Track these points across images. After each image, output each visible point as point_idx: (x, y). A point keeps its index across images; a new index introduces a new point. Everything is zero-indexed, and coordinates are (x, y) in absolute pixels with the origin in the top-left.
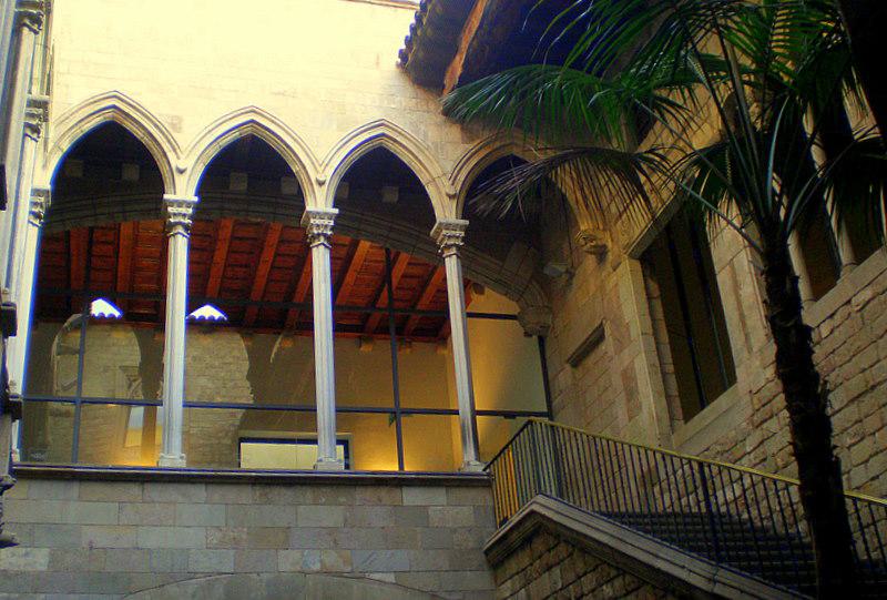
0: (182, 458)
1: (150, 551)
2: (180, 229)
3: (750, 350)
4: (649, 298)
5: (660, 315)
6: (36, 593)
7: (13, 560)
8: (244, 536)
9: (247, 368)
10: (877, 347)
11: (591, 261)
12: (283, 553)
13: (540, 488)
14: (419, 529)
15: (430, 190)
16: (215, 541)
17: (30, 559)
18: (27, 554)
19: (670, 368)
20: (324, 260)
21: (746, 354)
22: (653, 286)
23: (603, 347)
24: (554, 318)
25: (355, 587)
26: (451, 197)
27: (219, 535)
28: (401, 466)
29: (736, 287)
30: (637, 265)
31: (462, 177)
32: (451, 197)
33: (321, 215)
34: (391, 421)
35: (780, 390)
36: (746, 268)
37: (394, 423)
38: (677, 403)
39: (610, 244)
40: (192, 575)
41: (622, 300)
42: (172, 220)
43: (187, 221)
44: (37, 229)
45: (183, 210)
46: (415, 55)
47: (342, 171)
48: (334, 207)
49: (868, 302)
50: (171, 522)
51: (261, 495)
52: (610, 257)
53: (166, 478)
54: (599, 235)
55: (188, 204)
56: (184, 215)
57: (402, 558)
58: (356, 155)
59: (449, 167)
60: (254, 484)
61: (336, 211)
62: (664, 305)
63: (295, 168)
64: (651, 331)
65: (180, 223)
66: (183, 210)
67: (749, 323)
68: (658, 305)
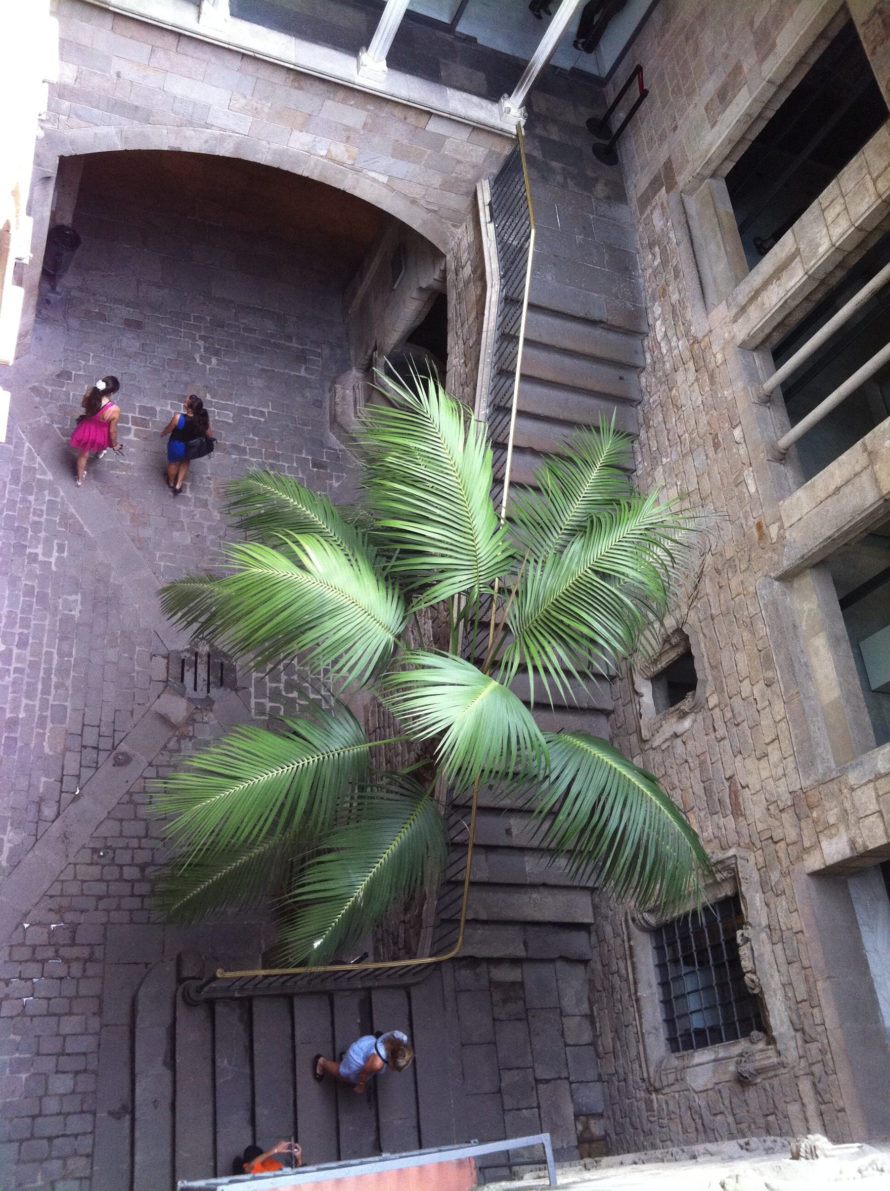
8: (266, 110)
12: (296, 133)
14: (429, 151)
16: (237, 106)
19: (770, 114)
25: (350, 176)
40: (208, 126)
57: (402, 168)
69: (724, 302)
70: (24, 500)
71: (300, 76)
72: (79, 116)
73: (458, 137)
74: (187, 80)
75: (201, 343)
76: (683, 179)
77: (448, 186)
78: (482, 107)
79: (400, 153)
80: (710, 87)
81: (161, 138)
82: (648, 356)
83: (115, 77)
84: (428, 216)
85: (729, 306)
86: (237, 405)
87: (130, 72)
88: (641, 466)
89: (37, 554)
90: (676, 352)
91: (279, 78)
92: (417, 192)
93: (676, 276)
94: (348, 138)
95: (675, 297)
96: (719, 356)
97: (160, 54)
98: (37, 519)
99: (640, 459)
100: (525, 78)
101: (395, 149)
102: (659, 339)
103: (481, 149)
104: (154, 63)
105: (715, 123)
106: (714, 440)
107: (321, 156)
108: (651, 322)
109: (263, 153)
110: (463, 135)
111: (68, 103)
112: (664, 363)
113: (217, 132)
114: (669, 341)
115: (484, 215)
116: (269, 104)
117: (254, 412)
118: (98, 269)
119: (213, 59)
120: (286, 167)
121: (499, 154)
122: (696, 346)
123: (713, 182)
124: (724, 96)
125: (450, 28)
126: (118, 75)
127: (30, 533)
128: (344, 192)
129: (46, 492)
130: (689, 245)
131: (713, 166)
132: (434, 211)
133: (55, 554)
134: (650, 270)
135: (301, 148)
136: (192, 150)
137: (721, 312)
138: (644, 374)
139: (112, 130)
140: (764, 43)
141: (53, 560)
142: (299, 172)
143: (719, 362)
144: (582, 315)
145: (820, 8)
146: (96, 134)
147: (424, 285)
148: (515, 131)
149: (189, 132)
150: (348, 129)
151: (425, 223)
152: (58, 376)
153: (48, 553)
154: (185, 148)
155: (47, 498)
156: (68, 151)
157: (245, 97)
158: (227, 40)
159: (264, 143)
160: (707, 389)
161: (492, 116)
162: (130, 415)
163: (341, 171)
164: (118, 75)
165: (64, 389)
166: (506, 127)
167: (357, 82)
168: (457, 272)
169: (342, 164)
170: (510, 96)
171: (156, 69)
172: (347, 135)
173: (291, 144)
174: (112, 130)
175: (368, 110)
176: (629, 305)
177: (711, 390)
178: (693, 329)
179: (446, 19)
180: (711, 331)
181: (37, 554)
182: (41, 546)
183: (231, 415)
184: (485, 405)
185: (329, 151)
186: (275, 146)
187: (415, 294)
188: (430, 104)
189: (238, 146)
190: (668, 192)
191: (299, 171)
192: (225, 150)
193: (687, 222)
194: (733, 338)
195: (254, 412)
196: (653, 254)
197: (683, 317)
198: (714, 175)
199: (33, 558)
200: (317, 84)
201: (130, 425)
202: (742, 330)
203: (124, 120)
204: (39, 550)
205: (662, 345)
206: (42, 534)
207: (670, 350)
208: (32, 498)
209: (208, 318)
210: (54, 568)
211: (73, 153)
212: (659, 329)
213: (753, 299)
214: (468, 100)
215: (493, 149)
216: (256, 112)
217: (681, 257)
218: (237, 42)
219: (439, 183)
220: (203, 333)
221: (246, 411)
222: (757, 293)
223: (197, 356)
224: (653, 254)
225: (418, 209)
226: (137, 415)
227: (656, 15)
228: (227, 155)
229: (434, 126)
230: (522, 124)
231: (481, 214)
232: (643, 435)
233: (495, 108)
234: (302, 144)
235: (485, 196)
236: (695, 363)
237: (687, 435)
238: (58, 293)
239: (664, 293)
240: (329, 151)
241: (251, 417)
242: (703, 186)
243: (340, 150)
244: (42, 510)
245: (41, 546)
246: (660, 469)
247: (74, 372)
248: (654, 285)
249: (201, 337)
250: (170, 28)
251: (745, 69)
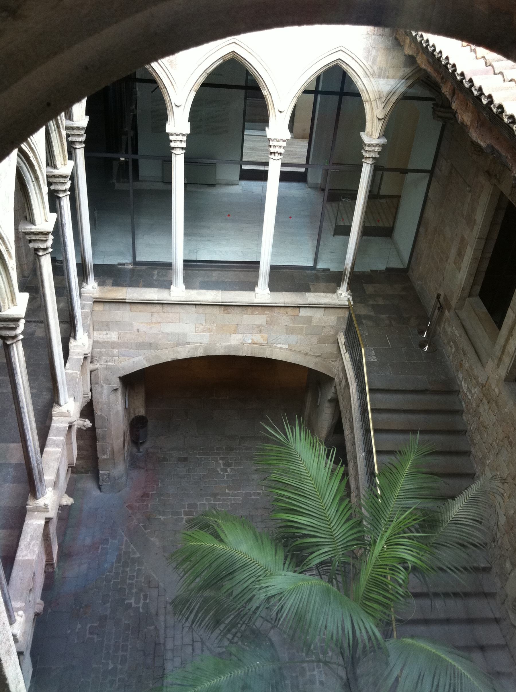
6: (114, 349)
7: (101, 336)
8: (214, 328)
12: (233, 336)
14: (305, 326)
16: (200, 330)
17: (109, 336)
18: (107, 334)
19: (489, 255)
20: (51, 290)
25: (267, 350)
35: (485, 237)
40: (188, 344)
44: (369, 166)
45: (180, 138)
57: (294, 338)
63: (265, 92)
66: (180, 138)
69: (490, 359)
70: (124, 571)
71: (226, 306)
72: (124, 355)
73: (318, 315)
74: (171, 324)
75: (221, 462)
76: (454, 302)
77: (322, 341)
78: (326, 297)
79: (290, 331)
80: (453, 252)
81: (167, 355)
82: (463, 403)
83: (136, 332)
84: (317, 359)
85: (493, 360)
86: (244, 492)
87: (143, 328)
88: (477, 470)
89: (131, 603)
90: (475, 395)
91: (216, 310)
92: (306, 348)
93: (465, 354)
94: (260, 331)
95: (467, 365)
96: (497, 390)
97: (155, 315)
98: (130, 581)
99: (476, 466)
100: (344, 276)
101: (287, 330)
102: (466, 392)
103: (333, 318)
104: (154, 320)
105: (460, 269)
106: (508, 440)
107: (250, 343)
108: (459, 383)
109: (219, 350)
110: (320, 313)
111: (117, 350)
112: (472, 404)
113: (193, 345)
114: (470, 391)
115: (343, 350)
116: (215, 325)
117: (254, 494)
118: (162, 435)
119: (182, 311)
120: (233, 354)
121: (344, 318)
122: (484, 389)
123: (471, 299)
124: (460, 254)
125: (314, 268)
126: (138, 330)
127: (127, 590)
128: (267, 358)
129: (136, 565)
130: (465, 335)
131: (467, 291)
132: (319, 356)
133: (142, 601)
134: (451, 356)
135: (237, 342)
136: (183, 358)
137: (490, 365)
138: (464, 414)
139: (141, 358)
140: (470, 221)
141: (140, 605)
142: (240, 355)
143: (498, 393)
144: (412, 389)
145: (490, 196)
146: (134, 362)
147: (329, 398)
148: (347, 303)
149: (179, 349)
150: (259, 326)
151: (316, 363)
152: (142, 496)
153: (137, 602)
154: (179, 358)
155: (137, 568)
156: (122, 373)
157: (203, 325)
158: (184, 300)
159: (218, 344)
160: (496, 411)
161: (333, 300)
162: (183, 510)
163: (262, 348)
164: (138, 330)
165: (145, 503)
166: (341, 303)
167: (255, 302)
168: (340, 384)
169: (261, 344)
170: (340, 287)
171: (155, 323)
172: (260, 329)
173: (232, 342)
174: (141, 358)
175: (266, 314)
176: (443, 377)
177: (499, 411)
178: (480, 380)
179: (311, 264)
180: (488, 378)
181: (131, 603)
182: (133, 598)
183: (241, 499)
184: (361, 451)
185: (253, 340)
186: (224, 345)
187: (327, 405)
188: (296, 303)
189: (205, 349)
190: (449, 312)
191: (240, 354)
192: (200, 353)
193: (462, 324)
194: (500, 377)
195: (254, 494)
196: (451, 347)
197: (473, 375)
198: (470, 295)
199: (129, 606)
200: (236, 308)
201: (183, 516)
202: (503, 372)
203: (145, 352)
204: (133, 601)
205: (468, 394)
206: (134, 591)
207: (472, 396)
208: (128, 569)
209: (224, 447)
210: (141, 610)
211: (125, 374)
212: (464, 386)
213: (503, 352)
214: (318, 296)
215: (339, 316)
216: (210, 330)
217: (464, 344)
218: (190, 299)
219: (317, 341)
220: (222, 456)
221: (250, 495)
222: (504, 347)
223: (219, 470)
224: (451, 347)
225: (309, 357)
226: (186, 510)
227: (422, 230)
228: (201, 355)
229: (303, 313)
230: (351, 299)
231: (341, 350)
232: (472, 450)
233: (334, 296)
234: (237, 340)
235: (342, 340)
236: (487, 398)
237: (494, 443)
238: (141, 452)
239: (461, 365)
240: (253, 340)
241: (253, 497)
242: (466, 302)
243: (258, 338)
244: (133, 576)
245: (133, 598)
246: (487, 468)
247: (150, 493)
248: (455, 363)
249: (221, 459)
250: (156, 302)
251: (466, 237)
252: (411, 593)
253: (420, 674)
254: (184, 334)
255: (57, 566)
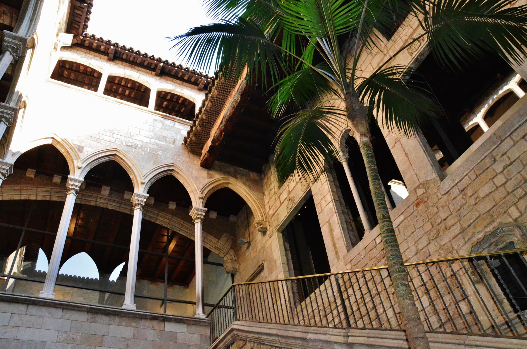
0: (53, 294)
1: (23, 341)
2: (73, 191)
3: (338, 258)
4: (286, 250)
5: (290, 258)
8: (79, 338)
9: (98, 297)
10: (408, 242)
11: (259, 235)
13: (236, 317)
14: (171, 343)
15: (191, 196)
16: (62, 339)
21: (336, 261)
22: (288, 246)
23: (262, 274)
24: (240, 265)
26: (201, 198)
27: (65, 335)
28: (165, 311)
29: (331, 230)
30: (281, 234)
31: (206, 192)
32: (201, 198)
33: (141, 196)
34: (162, 304)
36: (337, 222)
37: (163, 306)
38: (297, 295)
39: (268, 227)
41: (273, 250)
42: (70, 187)
43: (77, 188)
45: (77, 184)
46: (191, 140)
47: (153, 181)
48: (147, 193)
49: (402, 222)
50: (39, 327)
51: (91, 318)
52: (268, 233)
53: (41, 303)
54: (264, 223)
55: (79, 182)
56: (76, 186)
58: (160, 176)
59: (201, 186)
60: (88, 312)
61: (148, 195)
62: (291, 253)
64: (286, 263)
65: (73, 189)
67: (338, 246)
68: (289, 253)
97: (16, 317)
103: (196, 335)
157: (66, 333)
229: (169, 327)
252: (271, 244)
253: (31, 21)
254: (42, 342)
255: (516, 22)
